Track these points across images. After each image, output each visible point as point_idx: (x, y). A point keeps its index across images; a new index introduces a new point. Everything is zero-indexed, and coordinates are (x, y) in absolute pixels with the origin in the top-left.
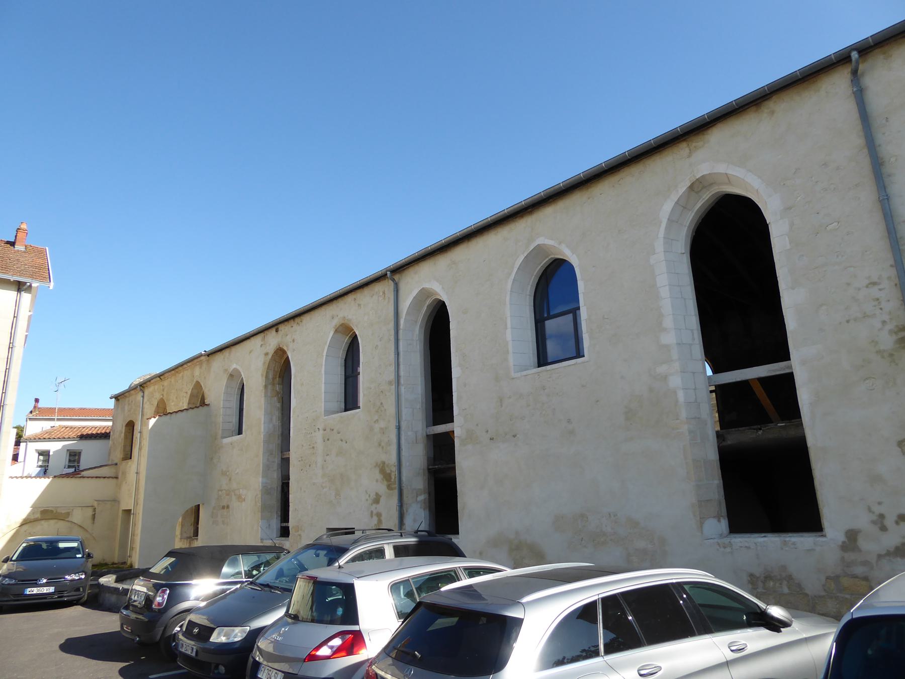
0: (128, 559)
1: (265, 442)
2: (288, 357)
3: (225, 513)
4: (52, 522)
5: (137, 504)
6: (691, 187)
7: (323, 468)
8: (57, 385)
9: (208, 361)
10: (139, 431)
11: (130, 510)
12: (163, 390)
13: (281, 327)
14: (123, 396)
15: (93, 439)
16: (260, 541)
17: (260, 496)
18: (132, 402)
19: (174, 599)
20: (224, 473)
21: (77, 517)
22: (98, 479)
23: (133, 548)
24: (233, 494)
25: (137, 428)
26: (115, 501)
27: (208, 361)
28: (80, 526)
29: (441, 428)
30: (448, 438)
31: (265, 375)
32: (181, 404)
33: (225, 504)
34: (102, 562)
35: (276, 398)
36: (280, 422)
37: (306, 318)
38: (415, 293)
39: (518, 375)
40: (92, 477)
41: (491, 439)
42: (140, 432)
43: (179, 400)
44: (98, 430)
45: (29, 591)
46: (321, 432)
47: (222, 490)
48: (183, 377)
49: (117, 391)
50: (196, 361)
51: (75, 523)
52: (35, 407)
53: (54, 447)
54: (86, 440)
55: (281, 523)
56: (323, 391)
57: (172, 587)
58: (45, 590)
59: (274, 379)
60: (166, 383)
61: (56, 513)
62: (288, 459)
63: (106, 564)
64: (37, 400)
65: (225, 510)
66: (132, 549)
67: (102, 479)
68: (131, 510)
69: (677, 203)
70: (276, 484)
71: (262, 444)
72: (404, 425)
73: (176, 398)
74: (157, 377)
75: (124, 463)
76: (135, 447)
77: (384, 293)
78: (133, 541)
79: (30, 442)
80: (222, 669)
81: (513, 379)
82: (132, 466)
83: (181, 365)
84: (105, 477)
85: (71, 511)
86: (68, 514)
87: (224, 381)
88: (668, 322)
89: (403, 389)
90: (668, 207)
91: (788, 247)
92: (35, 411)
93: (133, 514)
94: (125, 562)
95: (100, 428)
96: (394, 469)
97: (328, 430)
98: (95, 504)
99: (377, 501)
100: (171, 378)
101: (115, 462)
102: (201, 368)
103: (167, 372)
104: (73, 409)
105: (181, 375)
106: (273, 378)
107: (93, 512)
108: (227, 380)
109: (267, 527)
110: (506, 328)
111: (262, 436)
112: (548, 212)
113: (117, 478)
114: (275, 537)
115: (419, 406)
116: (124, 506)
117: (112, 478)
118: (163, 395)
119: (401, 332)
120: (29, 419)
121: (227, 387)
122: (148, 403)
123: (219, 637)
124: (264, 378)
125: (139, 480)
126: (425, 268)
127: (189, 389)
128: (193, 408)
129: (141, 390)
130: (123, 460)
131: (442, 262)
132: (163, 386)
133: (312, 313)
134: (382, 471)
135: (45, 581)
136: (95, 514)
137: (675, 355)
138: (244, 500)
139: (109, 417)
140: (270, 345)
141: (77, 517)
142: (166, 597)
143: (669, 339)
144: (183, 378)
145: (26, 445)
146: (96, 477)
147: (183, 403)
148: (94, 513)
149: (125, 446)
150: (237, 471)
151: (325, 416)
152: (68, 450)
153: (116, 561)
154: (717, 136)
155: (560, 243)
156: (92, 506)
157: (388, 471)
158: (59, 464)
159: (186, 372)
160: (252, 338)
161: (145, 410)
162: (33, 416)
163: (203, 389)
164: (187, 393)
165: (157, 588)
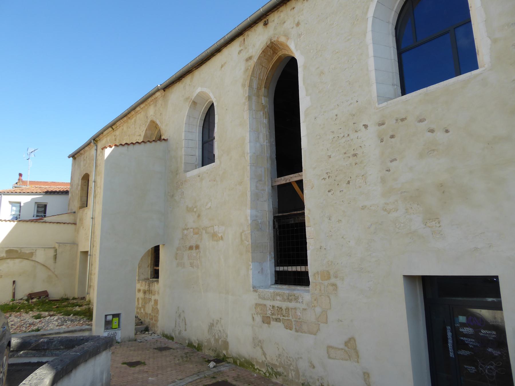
0: (86, 295)
1: (252, 165)
3: (195, 255)
4: (17, 261)
5: (94, 246)
8: (29, 154)
10: (94, 180)
11: (87, 252)
14: (79, 154)
16: (252, 289)
18: (87, 157)
20: (190, 210)
21: (40, 256)
22: (59, 224)
25: (92, 178)
26: (74, 244)
28: (44, 265)
31: (247, 83)
33: (193, 243)
34: (64, 297)
35: (262, 113)
36: (267, 141)
40: (54, 223)
42: (94, 182)
48: (135, 122)
49: (73, 150)
50: (150, 100)
52: (19, 179)
53: (25, 199)
54: (50, 194)
55: (275, 266)
59: (259, 89)
60: (117, 133)
61: (20, 253)
63: (67, 299)
64: (20, 175)
65: (194, 252)
66: (90, 287)
67: (62, 225)
68: (88, 251)
71: (249, 168)
75: (81, 211)
78: (90, 279)
79: (4, 195)
82: (88, 212)
83: (133, 108)
84: (65, 223)
85: (34, 251)
86: (32, 254)
92: (19, 182)
93: (90, 255)
94: (84, 297)
98: (57, 246)
100: (122, 126)
101: (74, 211)
102: (156, 105)
103: (119, 120)
104: (47, 182)
105: (133, 120)
106: (258, 87)
107: (54, 252)
108: (190, 107)
109: (259, 272)
113: (75, 224)
114: (270, 284)
116: (82, 249)
117: (71, 224)
120: (15, 187)
121: (189, 116)
124: (247, 88)
125: (94, 224)
132: (115, 136)
136: (56, 254)
138: (222, 238)
141: (40, 256)
145: (1, 197)
146: (57, 223)
148: (55, 254)
149: (81, 197)
150: (209, 205)
151: (379, 104)
152: (36, 203)
153: (76, 296)
158: (31, 213)
162: (18, 185)
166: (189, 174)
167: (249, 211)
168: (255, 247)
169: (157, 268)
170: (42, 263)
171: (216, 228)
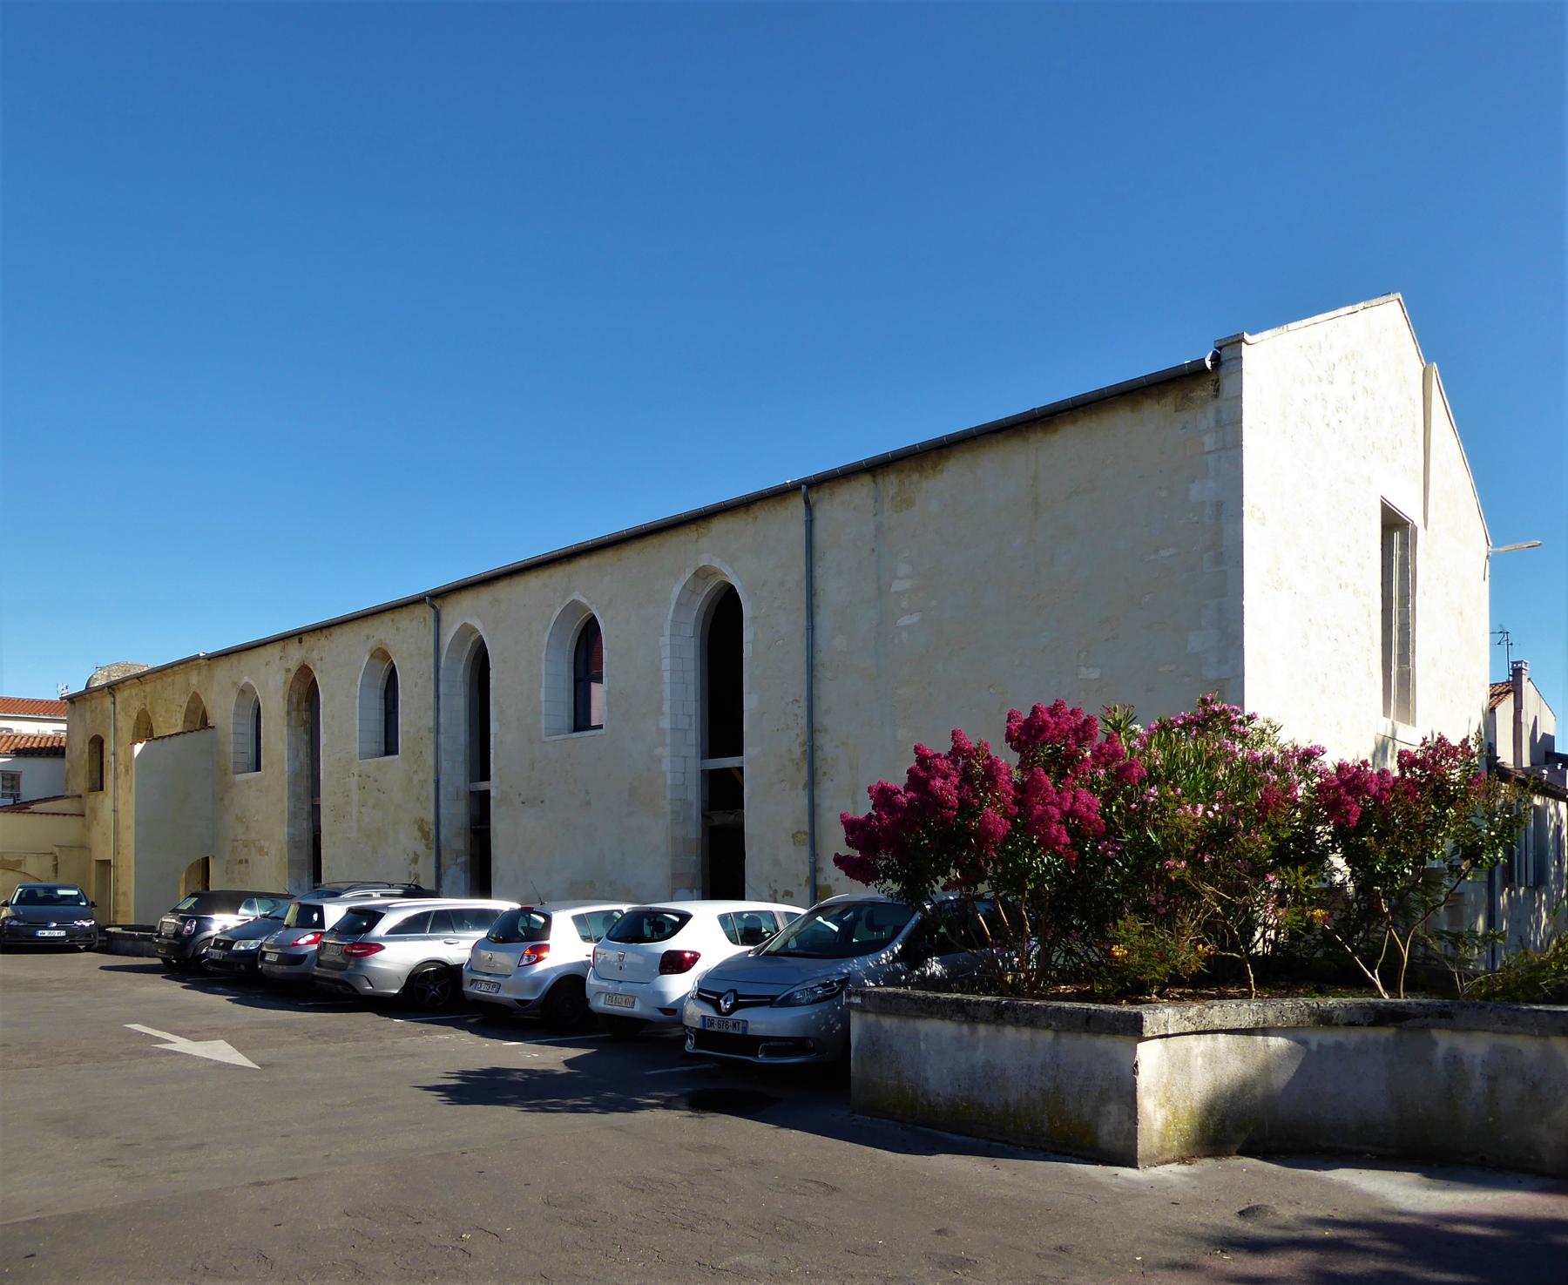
2: (315, 678)
5: (119, 853)
6: (696, 574)
7: (358, 821)
9: (209, 665)
12: (145, 697)
13: (306, 638)
15: (43, 757)
17: (286, 849)
18: (96, 708)
19: (201, 928)
22: (56, 816)
23: (117, 911)
24: (252, 845)
25: (109, 747)
26: (84, 847)
27: (209, 665)
29: (483, 786)
30: (484, 797)
32: (173, 720)
37: (337, 631)
38: (457, 627)
39: (547, 739)
41: (523, 803)
42: (114, 754)
43: (170, 720)
44: (40, 741)
45: (40, 933)
46: (356, 777)
47: (237, 841)
50: (191, 663)
51: (29, 875)
56: (357, 729)
57: (199, 919)
58: (56, 933)
59: (299, 703)
60: (148, 688)
62: (318, 806)
65: (244, 865)
69: (685, 586)
70: (306, 837)
72: (443, 779)
73: (166, 712)
74: (133, 678)
75: (92, 796)
76: (107, 774)
77: (425, 619)
80: (242, 967)
81: (545, 742)
82: (105, 801)
84: (65, 815)
86: (19, 863)
87: (233, 699)
88: (666, 707)
89: (442, 738)
90: (676, 590)
91: (751, 655)
95: (42, 738)
96: (433, 827)
97: (364, 777)
98: (56, 850)
99: (415, 860)
101: (78, 792)
105: (170, 680)
108: (238, 696)
110: (540, 687)
111: (287, 776)
112: (584, 564)
115: (461, 758)
118: (145, 704)
119: (441, 672)
122: (122, 713)
123: (240, 947)
124: (286, 702)
125: (118, 820)
126: (468, 600)
127: (184, 701)
128: (192, 732)
129: (110, 693)
130: (89, 792)
131: (486, 595)
133: (343, 626)
134: (421, 829)
135: (55, 925)
137: (668, 739)
139: (44, 714)
140: (292, 659)
142: (193, 926)
143: (666, 723)
144: (173, 684)
146: (53, 814)
147: (176, 720)
154: (719, 526)
155: (592, 603)
156: (51, 853)
157: (427, 830)
159: (177, 676)
160: (268, 646)
161: (119, 724)
163: (204, 703)
164: (181, 706)
165: (184, 920)
166: (240, 777)
167: (286, 829)
168: (292, 863)
169: (483, 786)
170: (37, 876)
171: (263, 843)
